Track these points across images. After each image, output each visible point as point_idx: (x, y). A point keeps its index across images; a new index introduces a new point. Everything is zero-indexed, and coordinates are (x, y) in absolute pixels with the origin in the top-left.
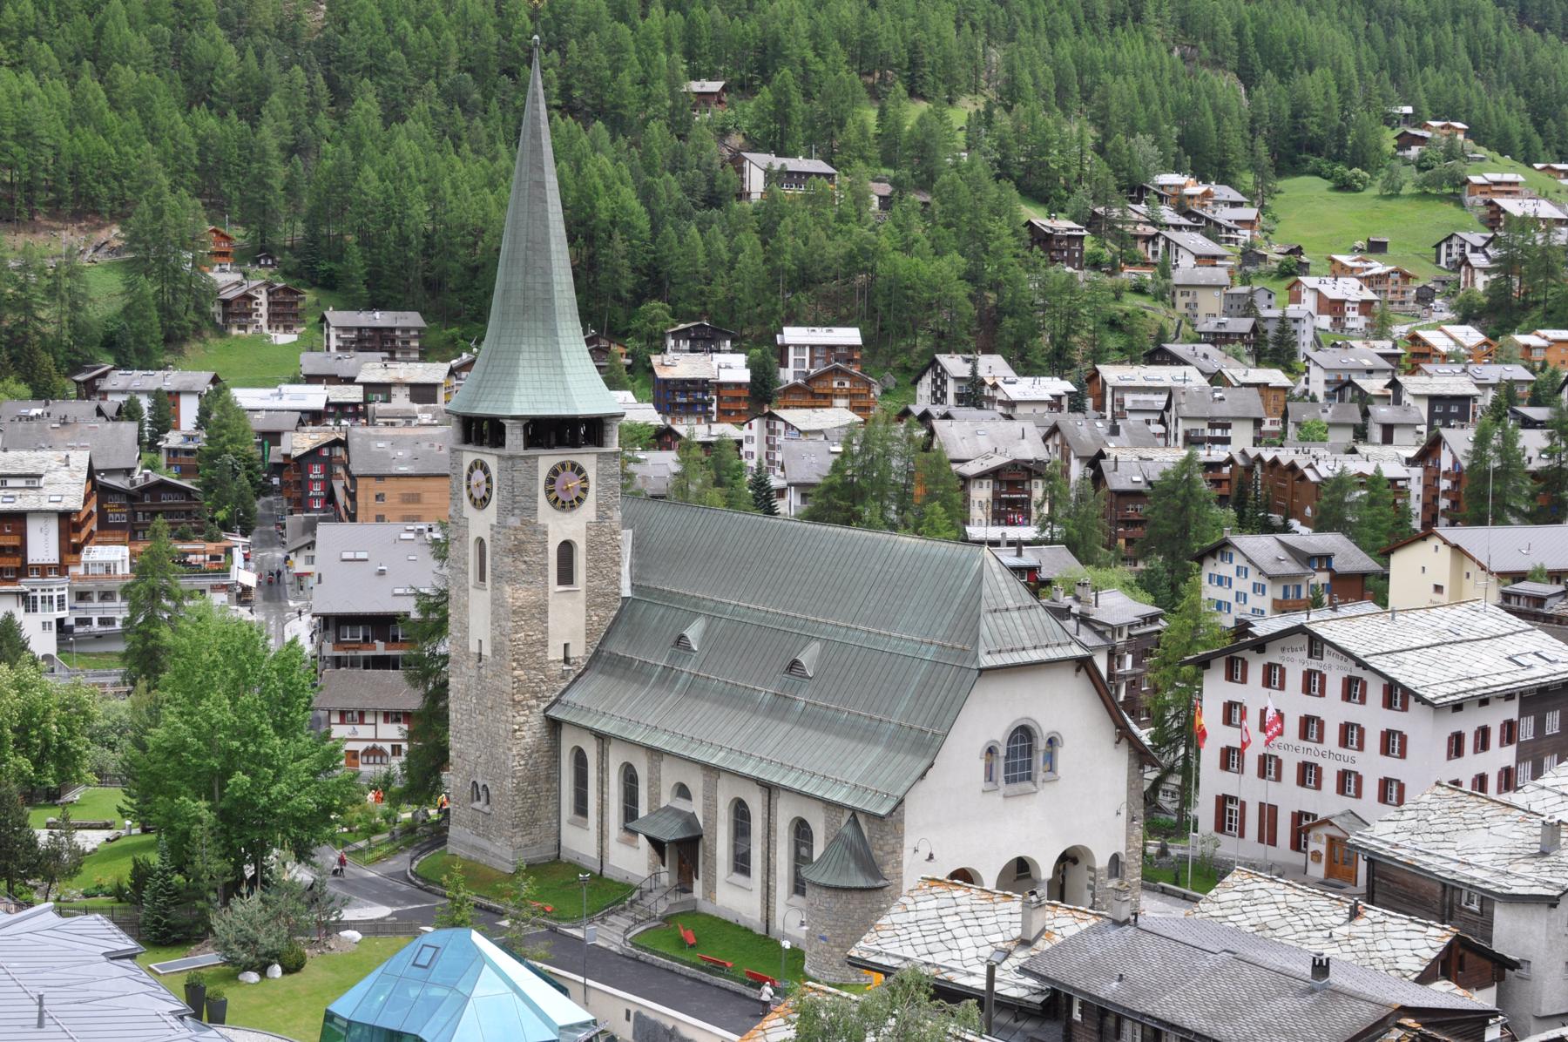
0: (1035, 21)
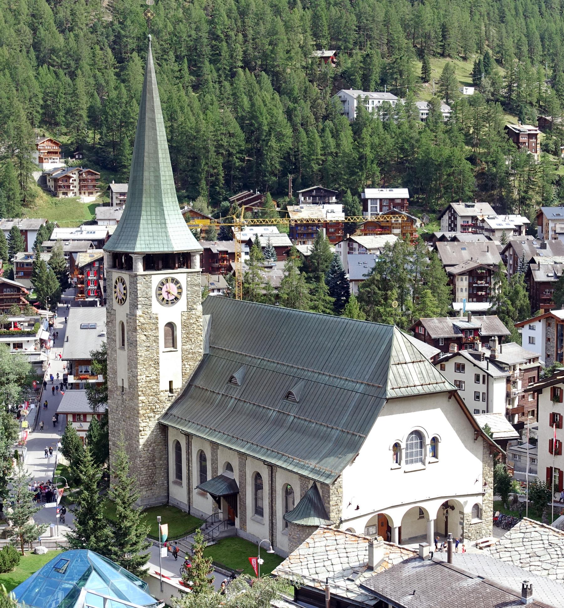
0: (516, 9)
